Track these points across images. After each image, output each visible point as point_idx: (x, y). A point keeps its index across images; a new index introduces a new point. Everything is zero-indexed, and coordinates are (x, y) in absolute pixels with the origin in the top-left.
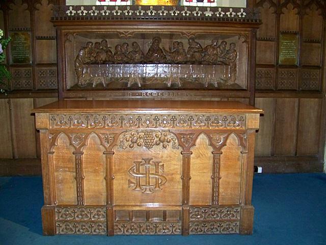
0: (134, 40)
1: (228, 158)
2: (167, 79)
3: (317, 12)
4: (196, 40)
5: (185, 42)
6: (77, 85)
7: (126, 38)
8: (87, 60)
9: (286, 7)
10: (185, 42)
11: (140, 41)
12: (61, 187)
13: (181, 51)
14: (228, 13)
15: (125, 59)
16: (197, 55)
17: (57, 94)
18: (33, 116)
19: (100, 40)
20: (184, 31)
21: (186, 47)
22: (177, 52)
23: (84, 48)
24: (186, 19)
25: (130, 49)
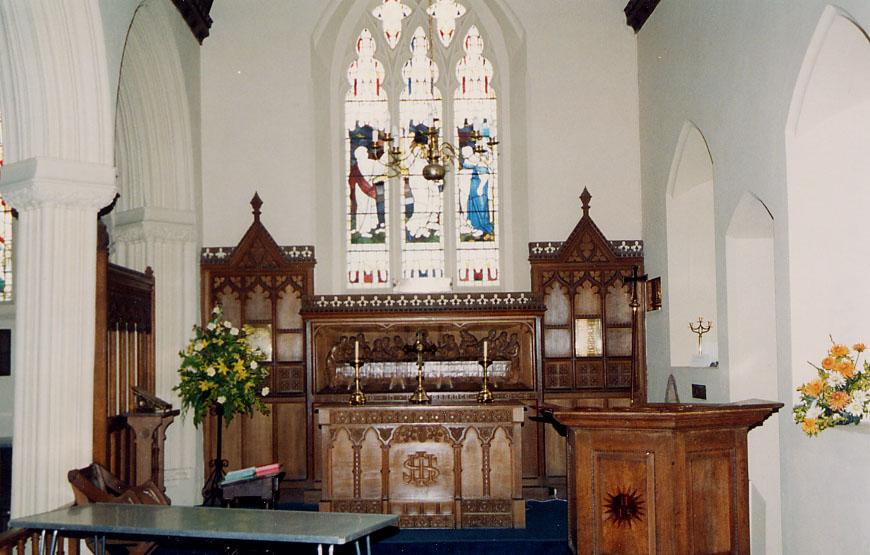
0: (397, 334)
1: (366, 482)
2: (436, 379)
3: (622, 290)
4: (470, 332)
5: (456, 334)
6: (327, 387)
7: (387, 331)
8: (340, 358)
9: (581, 285)
10: (456, 334)
11: (402, 335)
12: (641, 506)
13: (452, 345)
14: (479, 300)
15: (387, 356)
16: (471, 349)
17: (304, 399)
18: (323, 427)
19: (355, 335)
20: (523, 322)
21: (458, 341)
22: (450, 349)
23: (337, 344)
24: (495, 308)
25: (392, 344)
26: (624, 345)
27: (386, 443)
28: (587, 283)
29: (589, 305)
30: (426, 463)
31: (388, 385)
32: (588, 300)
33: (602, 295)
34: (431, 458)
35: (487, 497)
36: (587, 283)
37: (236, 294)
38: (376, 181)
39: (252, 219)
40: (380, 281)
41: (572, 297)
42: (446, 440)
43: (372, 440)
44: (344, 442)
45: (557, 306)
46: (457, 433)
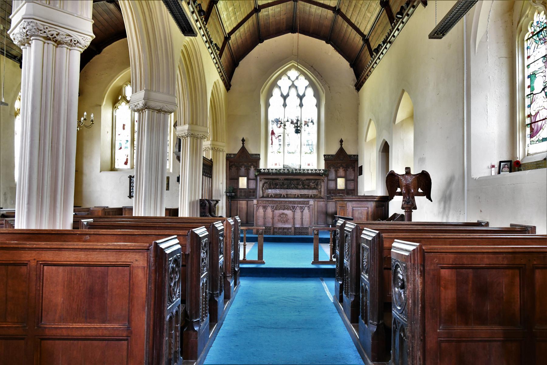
26: (351, 187)
27: (293, 210)
28: (341, 168)
29: (342, 174)
30: (284, 216)
31: (269, 196)
32: (341, 172)
33: (345, 171)
34: (286, 215)
35: (302, 226)
36: (341, 168)
37: (344, 169)
38: (279, 135)
39: (340, 146)
40: (312, 165)
41: (336, 172)
42: (291, 210)
43: (269, 210)
44: (261, 210)
45: (332, 175)
46: (294, 207)
